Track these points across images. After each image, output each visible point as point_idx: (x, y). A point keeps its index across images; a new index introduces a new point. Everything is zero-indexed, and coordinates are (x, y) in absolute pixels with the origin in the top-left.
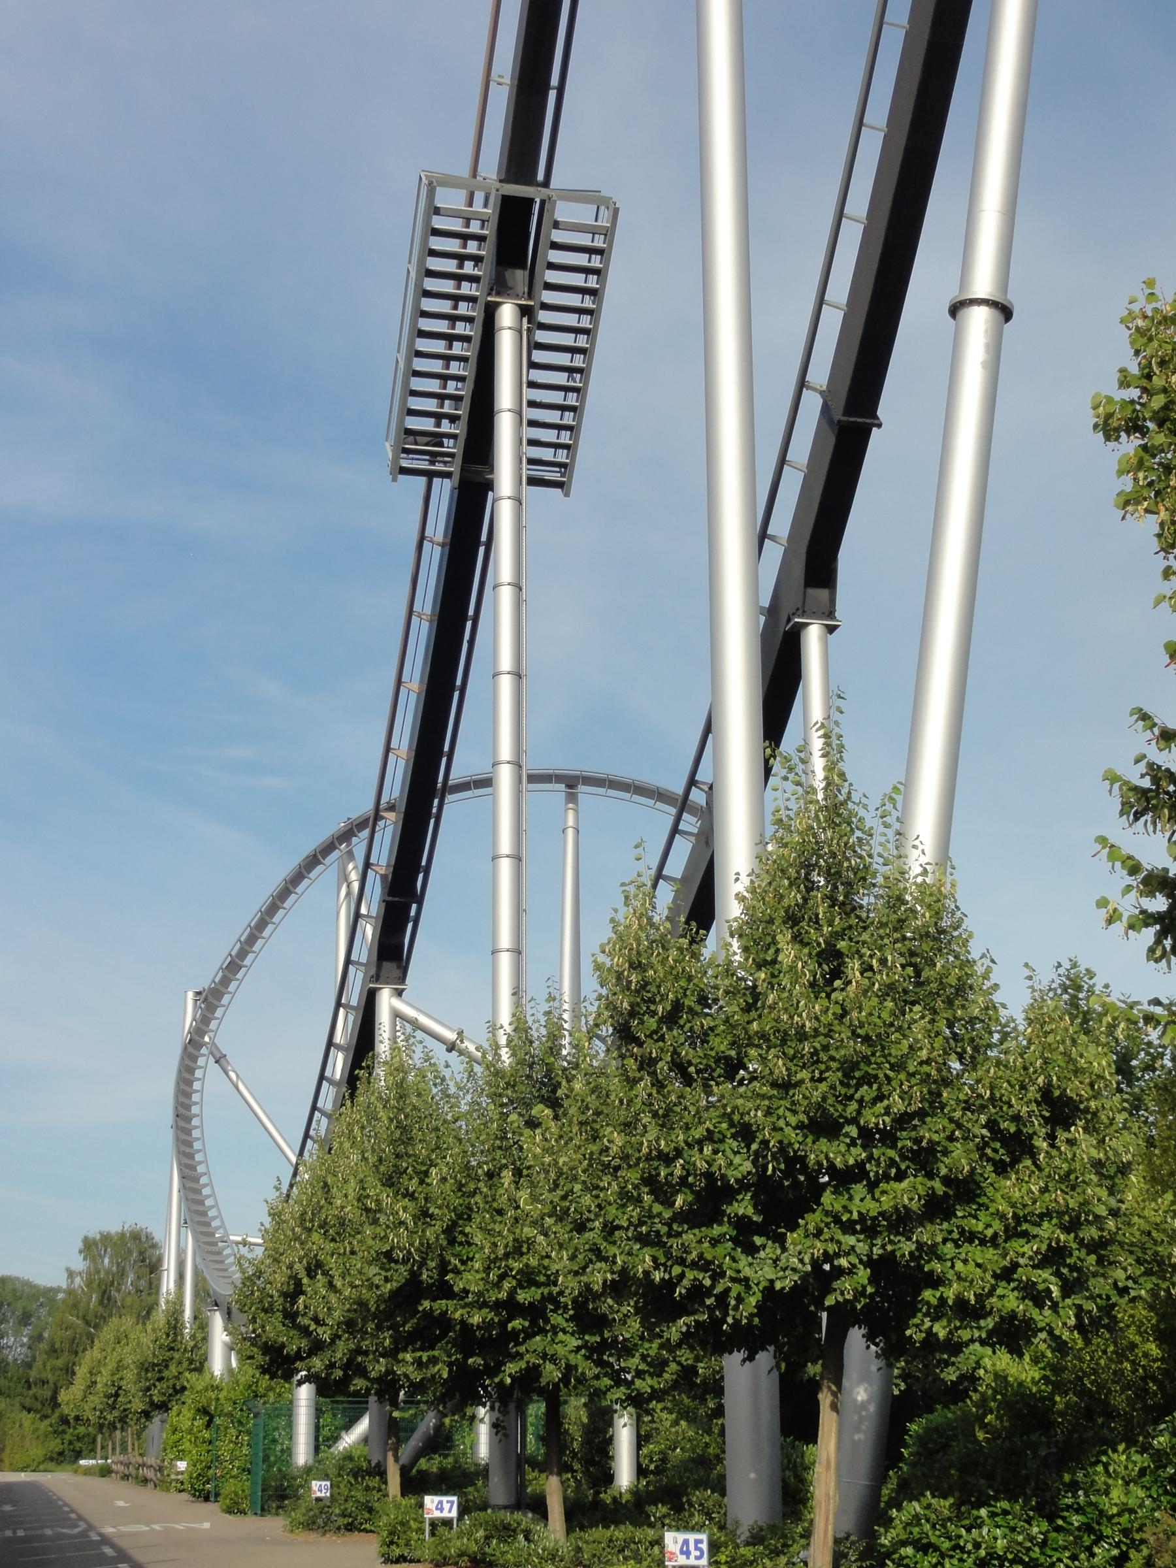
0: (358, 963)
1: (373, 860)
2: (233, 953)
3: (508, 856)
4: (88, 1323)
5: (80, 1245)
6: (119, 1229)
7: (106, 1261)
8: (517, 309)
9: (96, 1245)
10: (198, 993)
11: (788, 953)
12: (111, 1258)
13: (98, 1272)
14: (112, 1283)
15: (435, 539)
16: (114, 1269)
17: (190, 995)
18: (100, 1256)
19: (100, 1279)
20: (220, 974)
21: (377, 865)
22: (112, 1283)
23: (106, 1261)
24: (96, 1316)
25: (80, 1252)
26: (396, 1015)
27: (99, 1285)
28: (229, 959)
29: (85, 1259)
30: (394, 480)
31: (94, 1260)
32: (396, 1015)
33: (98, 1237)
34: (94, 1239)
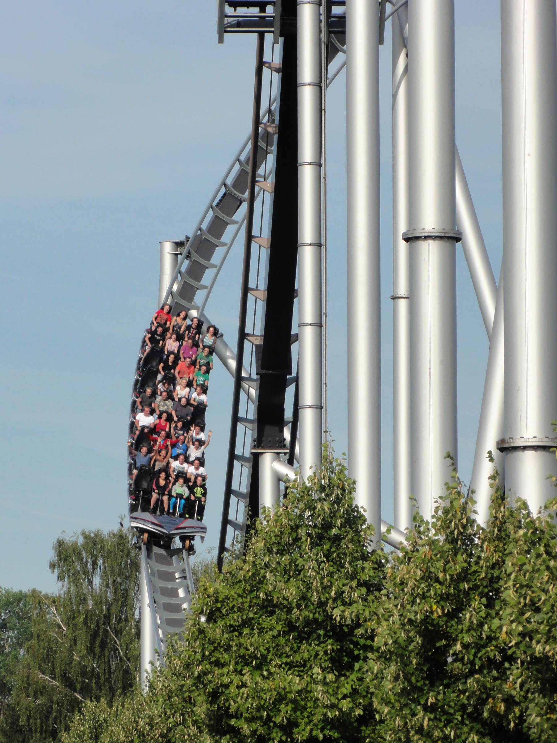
0: (246, 420)
1: (248, 330)
2: (229, 181)
3: (310, 407)
4: (69, 684)
5: (51, 555)
6: (115, 528)
7: (97, 580)
8: (174, 245)
9: (79, 554)
10: (179, 244)
11: (519, 503)
12: (104, 576)
13: (84, 600)
14: (108, 617)
15: (272, 65)
16: (110, 596)
17: (168, 247)
18: (86, 573)
19: (87, 612)
20: (211, 214)
21: (253, 335)
22: (108, 617)
23: (97, 580)
24: (84, 674)
25: (53, 566)
26: (278, 478)
27: (85, 622)
28: (223, 190)
29: (60, 578)
30: (221, 40)
31: (75, 580)
32: (278, 478)
33: (81, 541)
34: (75, 544)
